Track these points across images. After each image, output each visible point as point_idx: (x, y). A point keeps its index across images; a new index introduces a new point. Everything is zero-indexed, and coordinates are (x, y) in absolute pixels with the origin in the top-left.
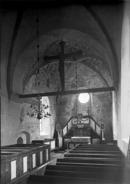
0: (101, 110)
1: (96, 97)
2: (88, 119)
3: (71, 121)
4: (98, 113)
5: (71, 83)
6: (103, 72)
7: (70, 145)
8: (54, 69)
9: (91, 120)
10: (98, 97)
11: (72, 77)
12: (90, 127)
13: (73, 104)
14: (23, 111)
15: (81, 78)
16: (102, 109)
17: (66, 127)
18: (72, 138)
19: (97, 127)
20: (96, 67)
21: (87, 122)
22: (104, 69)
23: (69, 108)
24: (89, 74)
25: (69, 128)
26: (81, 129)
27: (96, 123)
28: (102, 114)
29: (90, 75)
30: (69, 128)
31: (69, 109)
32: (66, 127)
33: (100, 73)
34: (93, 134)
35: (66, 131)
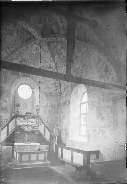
1: (44, 94)
3: (14, 120)
4: (44, 114)
6: (60, 67)
7: (23, 156)
8: (31, 61)
11: (17, 60)
12: (37, 131)
13: (12, 98)
14: (106, 165)
17: (6, 128)
18: (91, 168)
19: (46, 131)
20: (56, 57)
22: (63, 62)
23: (6, 101)
26: (27, 132)
31: (6, 103)
32: (6, 128)
33: (57, 66)
34: (40, 139)
35: (6, 136)
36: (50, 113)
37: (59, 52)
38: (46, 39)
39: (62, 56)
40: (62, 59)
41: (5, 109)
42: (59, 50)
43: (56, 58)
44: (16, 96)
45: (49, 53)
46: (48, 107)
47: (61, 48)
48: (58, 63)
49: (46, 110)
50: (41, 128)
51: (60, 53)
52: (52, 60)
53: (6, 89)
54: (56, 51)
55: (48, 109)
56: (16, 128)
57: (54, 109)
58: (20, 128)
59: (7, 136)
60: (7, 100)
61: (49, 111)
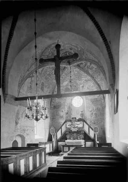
0: (94, 114)
2: (82, 122)
3: (65, 124)
4: (91, 117)
5: (65, 88)
6: (97, 77)
7: (65, 148)
9: (85, 123)
10: (91, 101)
15: (74, 82)
16: (95, 113)
21: (81, 126)
23: (62, 112)
24: (82, 79)
25: (63, 132)
26: (75, 132)
27: (90, 127)
28: (95, 117)
29: (84, 79)
30: (63, 132)
35: (60, 135)
36: (96, 116)
37: (90, 67)
38: (72, 65)
39: (94, 69)
40: (95, 71)
41: (62, 117)
42: (90, 66)
43: (90, 72)
44: (70, 108)
45: (81, 71)
46: (94, 111)
47: (91, 64)
48: (93, 75)
49: (93, 113)
50: (86, 128)
51: (91, 68)
52: (87, 75)
53: (62, 103)
54: (88, 68)
55: (94, 112)
56: (66, 129)
57: (100, 111)
58: (69, 129)
59: (61, 135)
60: (63, 111)
61: (96, 114)
